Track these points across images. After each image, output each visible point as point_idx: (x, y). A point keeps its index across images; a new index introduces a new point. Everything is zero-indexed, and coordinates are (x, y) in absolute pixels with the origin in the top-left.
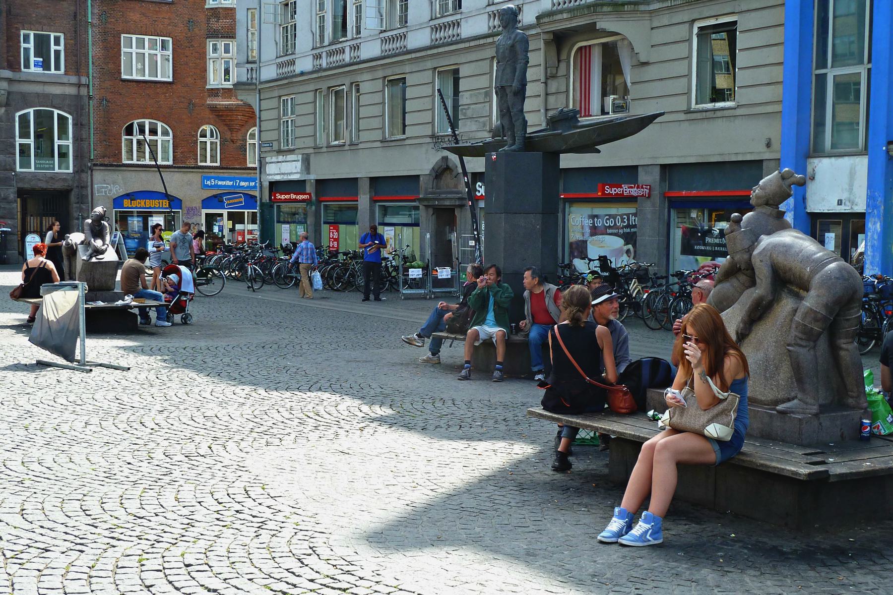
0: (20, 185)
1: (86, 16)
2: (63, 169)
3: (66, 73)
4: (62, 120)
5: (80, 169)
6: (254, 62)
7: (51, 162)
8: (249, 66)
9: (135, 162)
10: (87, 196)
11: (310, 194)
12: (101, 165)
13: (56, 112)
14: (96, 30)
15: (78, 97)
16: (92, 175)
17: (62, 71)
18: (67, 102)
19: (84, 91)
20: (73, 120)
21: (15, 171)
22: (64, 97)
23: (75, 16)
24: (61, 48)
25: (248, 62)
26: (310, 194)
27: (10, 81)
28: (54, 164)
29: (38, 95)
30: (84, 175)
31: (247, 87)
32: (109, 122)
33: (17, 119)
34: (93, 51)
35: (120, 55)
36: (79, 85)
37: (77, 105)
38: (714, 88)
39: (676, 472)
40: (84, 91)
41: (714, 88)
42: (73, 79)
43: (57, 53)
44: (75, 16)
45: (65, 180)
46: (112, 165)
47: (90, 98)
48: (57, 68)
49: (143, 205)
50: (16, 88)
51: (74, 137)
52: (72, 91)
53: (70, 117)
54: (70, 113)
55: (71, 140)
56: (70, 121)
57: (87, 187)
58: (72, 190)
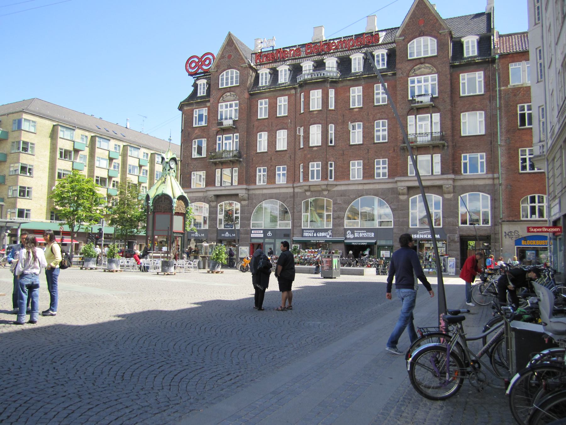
0: (461, 233)
1: (497, 142)
3: (487, 173)
5: (495, 224)
6: (544, 141)
8: (541, 144)
9: (529, 218)
10: (499, 239)
11: (560, 228)
12: (507, 221)
14: (504, 148)
15: (494, 185)
16: (501, 227)
17: (485, 172)
18: (487, 188)
19: (496, 182)
21: (458, 226)
22: (485, 185)
23: (491, 143)
25: (540, 141)
26: (560, 228)
27: (454, 180)
29: (470, 186)
30: (497, 227)
31: (539, 158)
34: (502, 159)
35: (518, 160)
36: (493, 179)
40: (496, 182)
42: (490, 176)
44: (491, 143)
45: (486, 230)
46: (514, 221)
49: (534, 243)
50: (458, 183)
52: (490, 182)
55: (490, 209)
57: (499, 233)
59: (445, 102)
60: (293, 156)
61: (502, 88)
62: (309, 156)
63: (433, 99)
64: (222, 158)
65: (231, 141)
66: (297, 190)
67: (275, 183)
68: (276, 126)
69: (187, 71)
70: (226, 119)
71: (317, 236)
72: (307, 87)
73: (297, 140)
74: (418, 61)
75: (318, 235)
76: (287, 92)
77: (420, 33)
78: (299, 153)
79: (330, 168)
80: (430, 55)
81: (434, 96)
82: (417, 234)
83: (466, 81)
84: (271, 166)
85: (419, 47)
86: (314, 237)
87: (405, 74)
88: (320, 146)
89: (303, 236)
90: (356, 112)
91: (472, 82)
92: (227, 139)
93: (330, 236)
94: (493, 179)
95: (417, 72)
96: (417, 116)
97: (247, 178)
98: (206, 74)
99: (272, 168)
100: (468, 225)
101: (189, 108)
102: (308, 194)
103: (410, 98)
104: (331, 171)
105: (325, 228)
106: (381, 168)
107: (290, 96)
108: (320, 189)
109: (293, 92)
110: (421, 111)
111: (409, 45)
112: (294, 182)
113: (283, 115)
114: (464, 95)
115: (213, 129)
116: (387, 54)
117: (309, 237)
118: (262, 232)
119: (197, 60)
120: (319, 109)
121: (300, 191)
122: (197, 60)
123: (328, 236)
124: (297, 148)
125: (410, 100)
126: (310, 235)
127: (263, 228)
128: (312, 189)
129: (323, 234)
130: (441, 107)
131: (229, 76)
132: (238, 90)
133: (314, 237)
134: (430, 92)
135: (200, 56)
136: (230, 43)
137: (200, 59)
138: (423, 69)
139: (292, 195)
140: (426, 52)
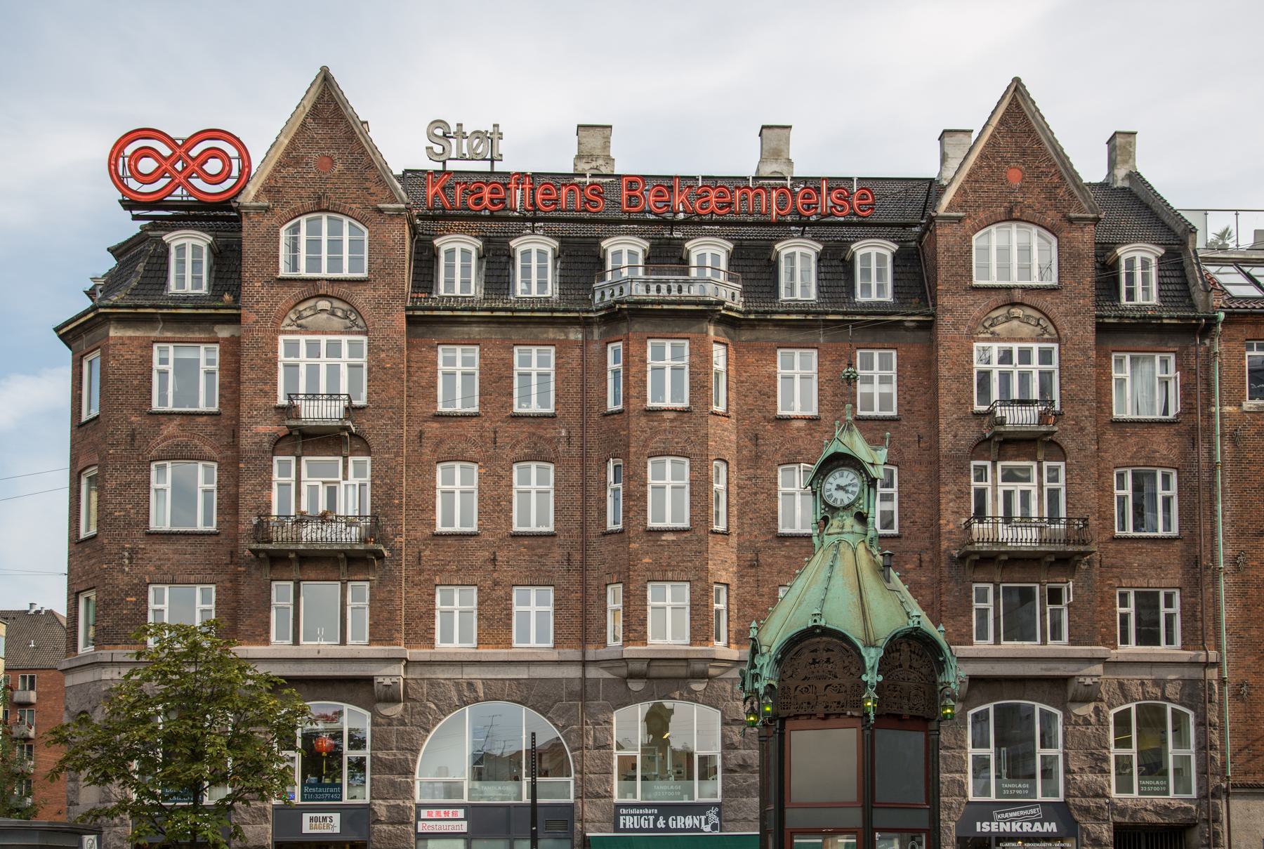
2: (1175, 797)
4: (1178, 718)
5: (1208, 795)
7: (1162, 783)
13: (1038, 706)
20: (1196, 717)
24: (1176, 609)
28: (1167, 786)
32: (1253, 718)
33: (970, 720)
36: (584, 663)
37: (1196, 694)
38: (417, 833)
39: (1054, 143)
41: (417, 833)
42: (573, 654)
43: (1170, 618)
47: (1222, 682)
48: (1170, 641)
51: (1198, 743)
52: (574, 672)
53: (1191, 714)
54: (1191, 708)
55: (1193, 749)
56: (1192, 720)
58: (1195, 825)
59: (1082, 429)
60: (577, 557)
61: (1228, 409)
62: (647, 560)
63: (351, 410)
64: (270, 542)
65: (1032, 487)
66: (593, 673)
67: (508, 644)
68: (513, 447)
69: (118, 181)
70: (313, 396)
71: (667, 829)
72: (637, 327)
73: (592, 501)
74: (1002, 297)
75: (672, 824)
76: (552, 333)
77: (1011, 211)
78: (602, 552)
79: (1120, 610)
80: (1036, 281)
81: (356, 403)
82: (991, 820)
83: (170, 367)
84: (496, 583)
85: (1004, 252)
86: (656, 829)
87: (964, 330)
88: (684, 531)
89: (617, 829)
90: (799, 430)
91: (186, 369)
92: (1009, 476)
93: (714, 827)
94: (584, 663)
95: (997, 329)
96: (304, 459)
97: (402, 620)
98: (218, 216)
99: (500, 592)
100: (1136, 794)
101: (130, 333)
102: (636, 686)
103: (282, 401)
104: (1124, 618)
105: (697, 799)
106: (534, 609)
107: (562, 348)
108: (682, 671)
109: (575, 335)
110: (1011, 450)
111: (974, 238)
112: (584, 641)
113: (534, 408)
114: (447, 410)
115: (262, 429)
116: (210, 246)
117: (641, 830)
118: (461, 813)
119: (165, 151)
120: (679, 405)
121: (607, 675)
122: (165, 151)
123: (707, 828)
124: (594, 530)
125: (283, 408)
126: (644, 824)
127: (465, 800)
128: (654, 672)
129: (689, 821)
130: (1068, 444)
131: (325, 237)
132: (362, 298)
133: (656, 829)
134: (344, 388)
135: (180, 132)
136: (327, 109)
137: (181, 148)
138: (1015, 323)
139: (577, 688)
140: (1025, 269)
